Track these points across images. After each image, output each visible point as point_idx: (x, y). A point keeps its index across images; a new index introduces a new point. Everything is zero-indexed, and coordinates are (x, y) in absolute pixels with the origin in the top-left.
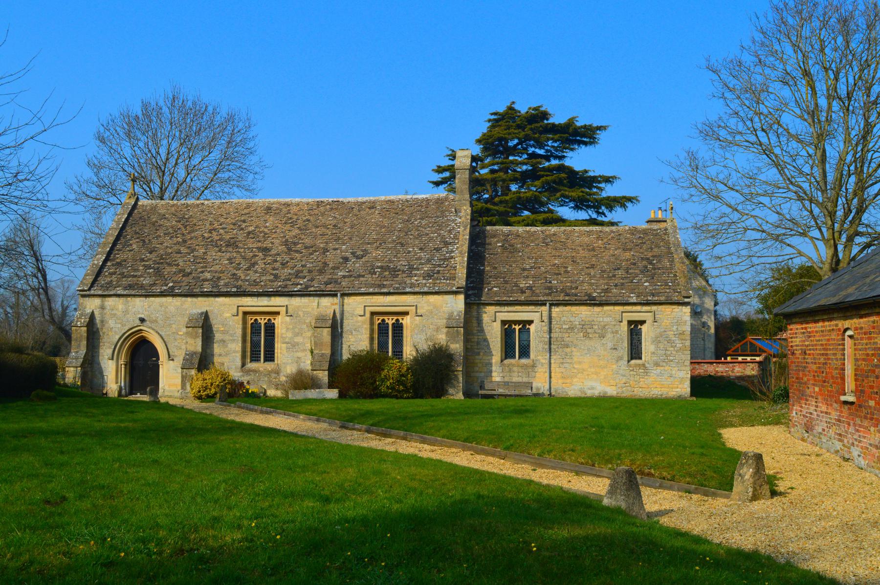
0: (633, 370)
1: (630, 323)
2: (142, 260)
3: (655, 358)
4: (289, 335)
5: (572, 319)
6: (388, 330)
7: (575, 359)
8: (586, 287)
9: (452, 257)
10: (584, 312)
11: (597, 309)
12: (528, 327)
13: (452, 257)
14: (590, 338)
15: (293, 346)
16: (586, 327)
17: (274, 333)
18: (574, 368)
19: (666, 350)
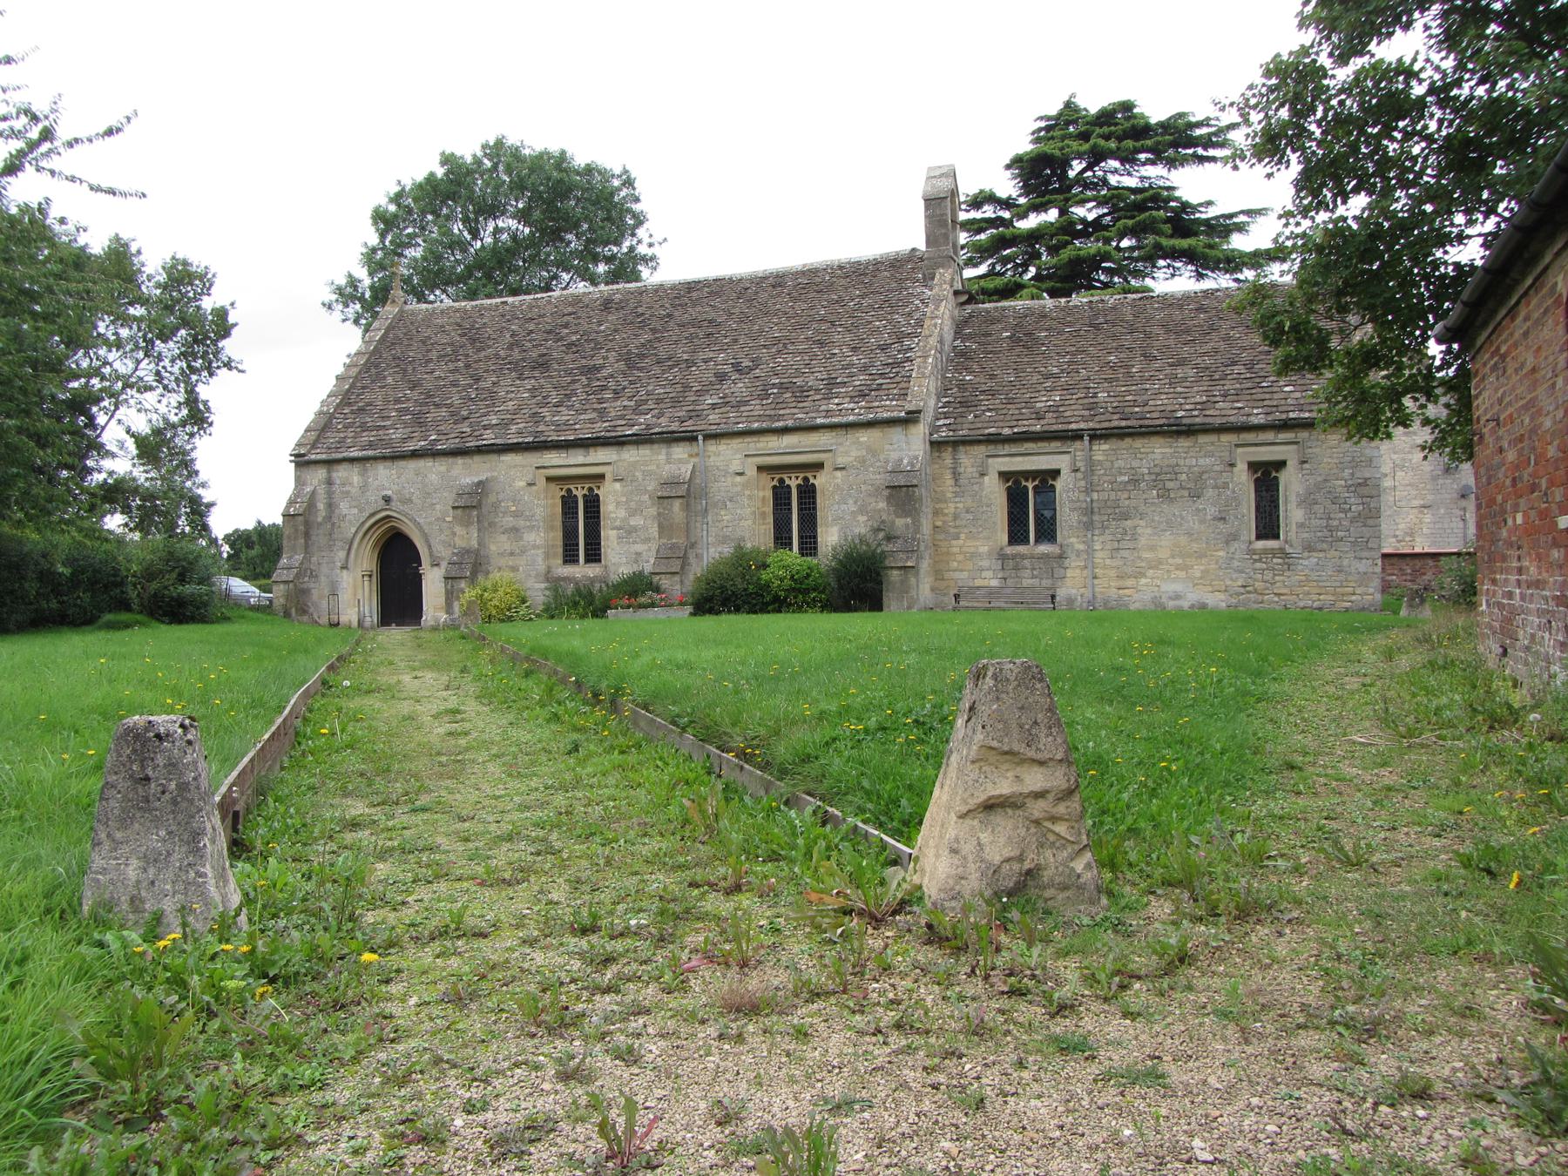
0: (1260, 560)
1: (1253, 466)
2: (397, 401)
3: (1306, 535)
4: (622, 513)
5: (1135, 464)
6: (789, 498)
7: (1143, 541)
8: (1162, 400)
9: (909, 360)
10: (1159, 451)
11: (1184, 443)
12: (1274, 474)
13: (909, 360)
14: (1172, 500)
15: (628, 532)
16: (1162, 477)
17: (599, 512)
18: (1139, 558)
19: (1330, 518)
